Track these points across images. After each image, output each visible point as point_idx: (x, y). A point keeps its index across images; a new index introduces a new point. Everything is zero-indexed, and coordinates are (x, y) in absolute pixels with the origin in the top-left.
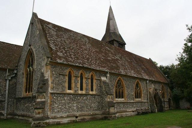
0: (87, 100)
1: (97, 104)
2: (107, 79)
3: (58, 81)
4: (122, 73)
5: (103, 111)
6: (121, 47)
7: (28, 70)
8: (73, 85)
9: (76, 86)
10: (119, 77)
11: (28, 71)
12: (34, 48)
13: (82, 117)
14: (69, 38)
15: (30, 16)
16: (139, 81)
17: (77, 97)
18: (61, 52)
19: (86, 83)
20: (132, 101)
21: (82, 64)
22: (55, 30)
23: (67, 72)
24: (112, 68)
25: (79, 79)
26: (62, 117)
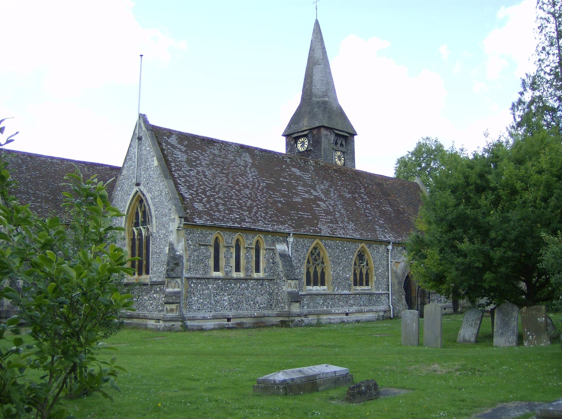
0: (247, 290)
1: (266, 297)
2: (288, 247)
3: (198, 256)
4: (323, 233)
5: (278, 310)
6: (341, 145)
7: (136, 231)
8: (222, 263)
9: (228, 264)
10: (315, 242)
11: (136, 234)
12: (150, 191)
13: (239, 321)
14: (212, 164)
15: (135, 119)
16: (366, 247)
17: (231, 284)
18: (201, 201)
19: (247, 258)
20: (346, 292)
21: (239, 223)
22: (183, 149)
23: (211, 239)
24: (299, 224)
25: (233, 250)
26: (204, 318)
